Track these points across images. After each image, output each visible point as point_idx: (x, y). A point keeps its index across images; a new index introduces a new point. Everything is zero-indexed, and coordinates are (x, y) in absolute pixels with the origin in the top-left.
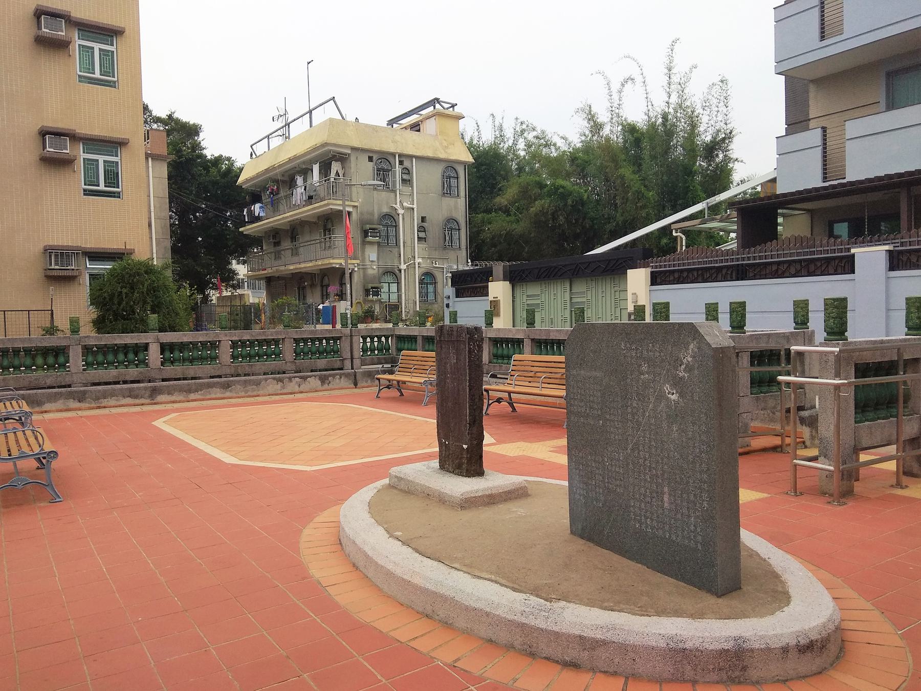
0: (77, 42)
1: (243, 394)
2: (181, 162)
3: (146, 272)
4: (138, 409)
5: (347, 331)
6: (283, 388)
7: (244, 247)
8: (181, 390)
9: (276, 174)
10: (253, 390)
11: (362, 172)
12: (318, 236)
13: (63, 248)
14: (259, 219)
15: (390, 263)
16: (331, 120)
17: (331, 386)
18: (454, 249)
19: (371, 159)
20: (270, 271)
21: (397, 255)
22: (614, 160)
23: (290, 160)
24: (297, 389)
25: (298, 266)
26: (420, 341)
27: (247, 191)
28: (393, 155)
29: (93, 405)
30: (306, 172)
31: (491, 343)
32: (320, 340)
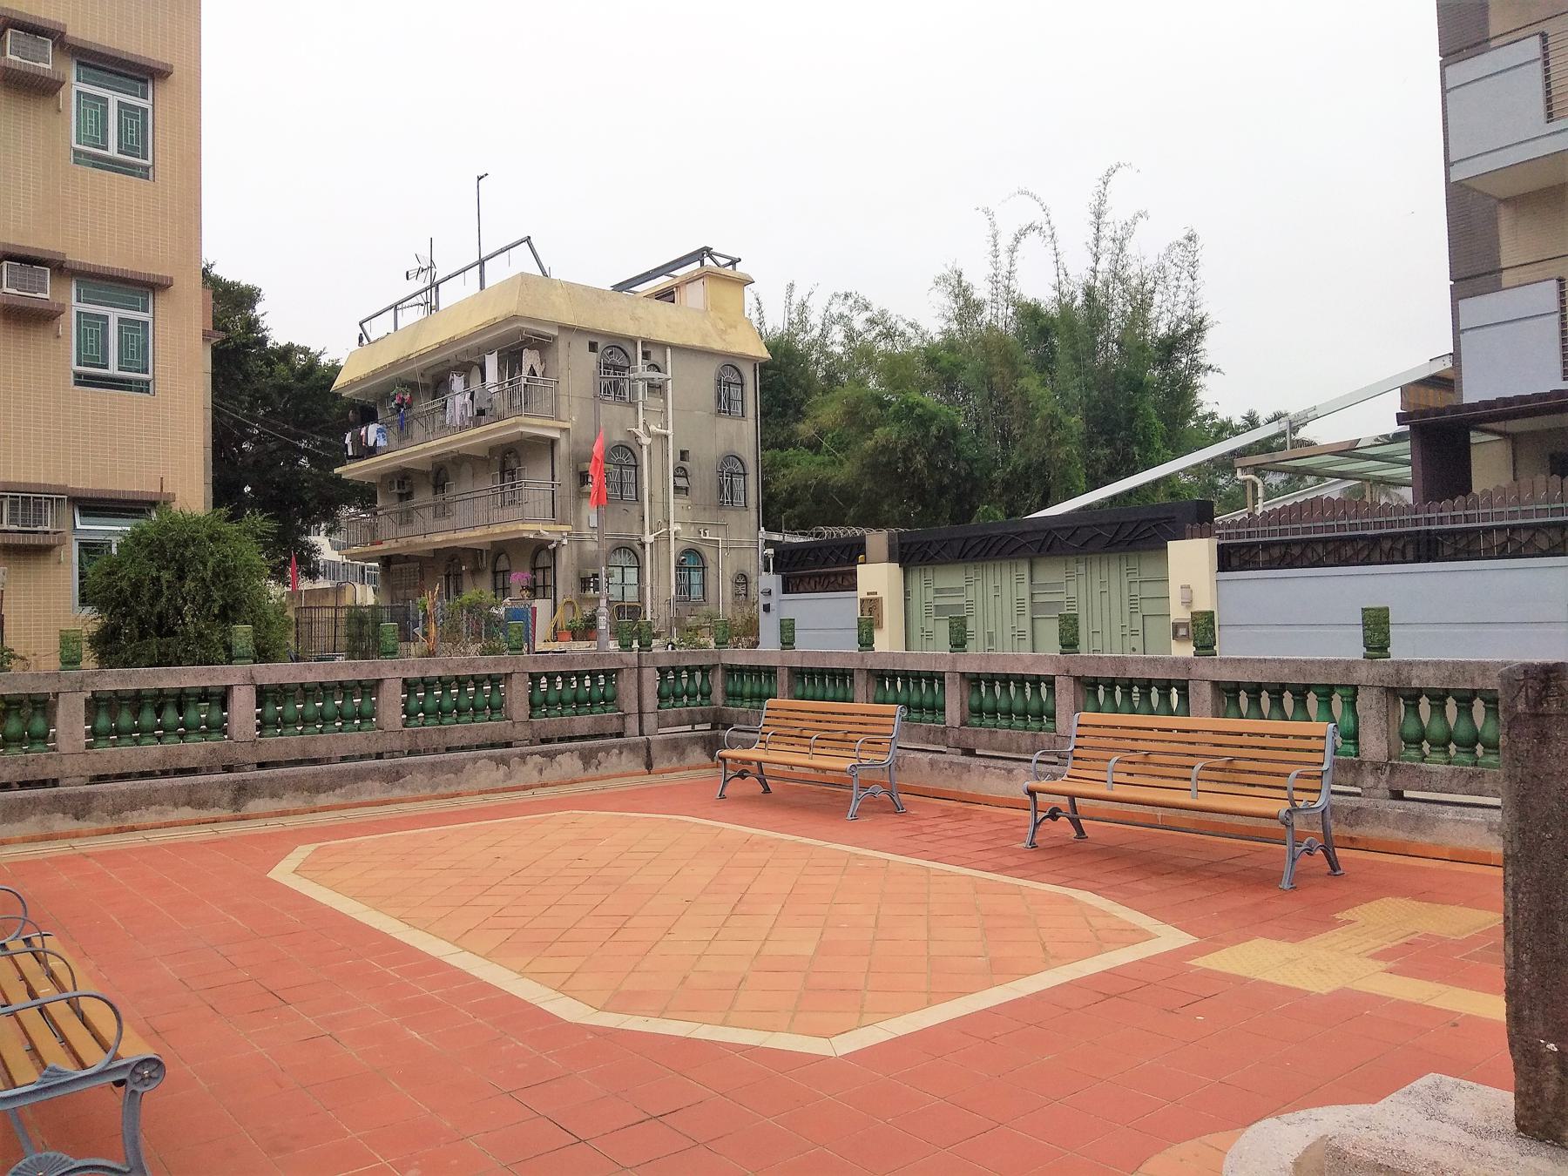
0: (75, 86)
1: (427, 792)
2: (226, 350)
3: (211, 538)
4: (204, 833)
5: (631, 658)
6: (509, 776)
7: (328, 500)
8: (298, 786)
9: (413, 372)
10: (449, 783)
11: (577, 370)
12: (489, 482)
13: (28, 488)
14: (372, 451)
15: (623, 527)
16: (524, 278)
17: (602, 770)
18: (736, 509)
19: (593, 347)
20: (393, 544)
21: (638, 518)
22: (1009, 360)
23: (442, 346)
24: (535, 778)
25: (452, 536)
26: (783, 677)
27: (352, 404)
28: (633, 341)
29: (107, 825)
30: (470, 366)
31: (965, 685)
32: (580, 676)
